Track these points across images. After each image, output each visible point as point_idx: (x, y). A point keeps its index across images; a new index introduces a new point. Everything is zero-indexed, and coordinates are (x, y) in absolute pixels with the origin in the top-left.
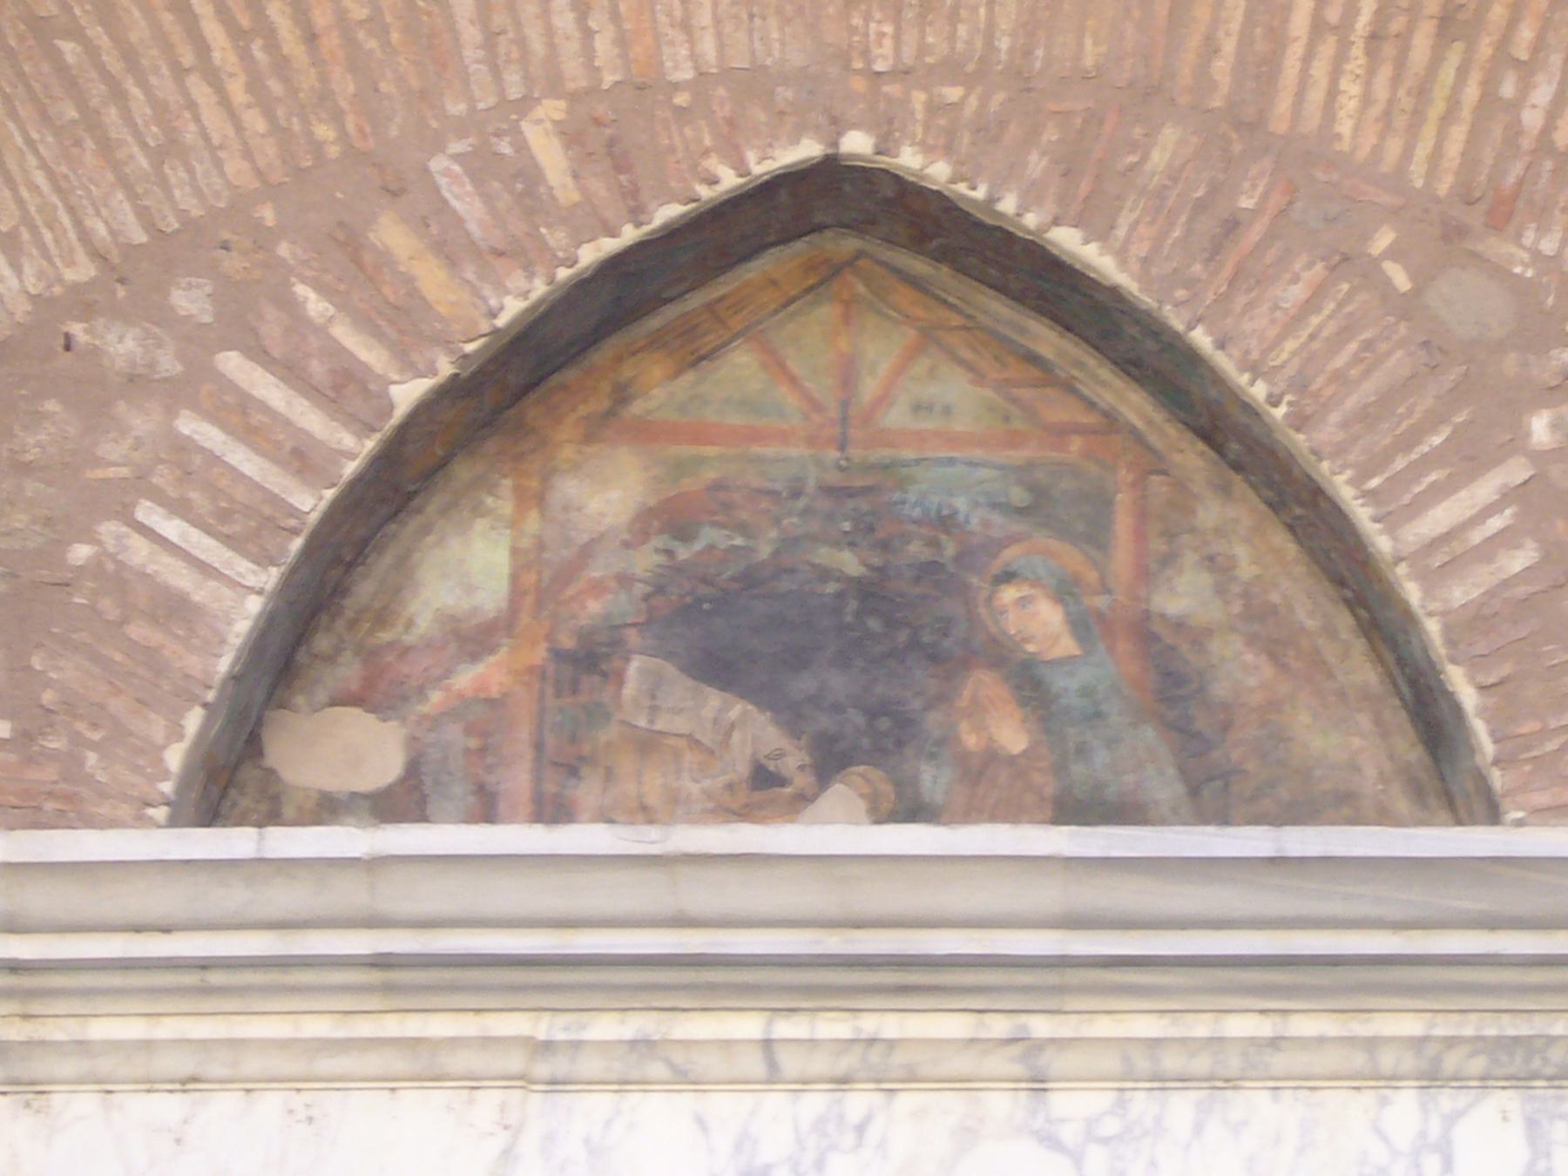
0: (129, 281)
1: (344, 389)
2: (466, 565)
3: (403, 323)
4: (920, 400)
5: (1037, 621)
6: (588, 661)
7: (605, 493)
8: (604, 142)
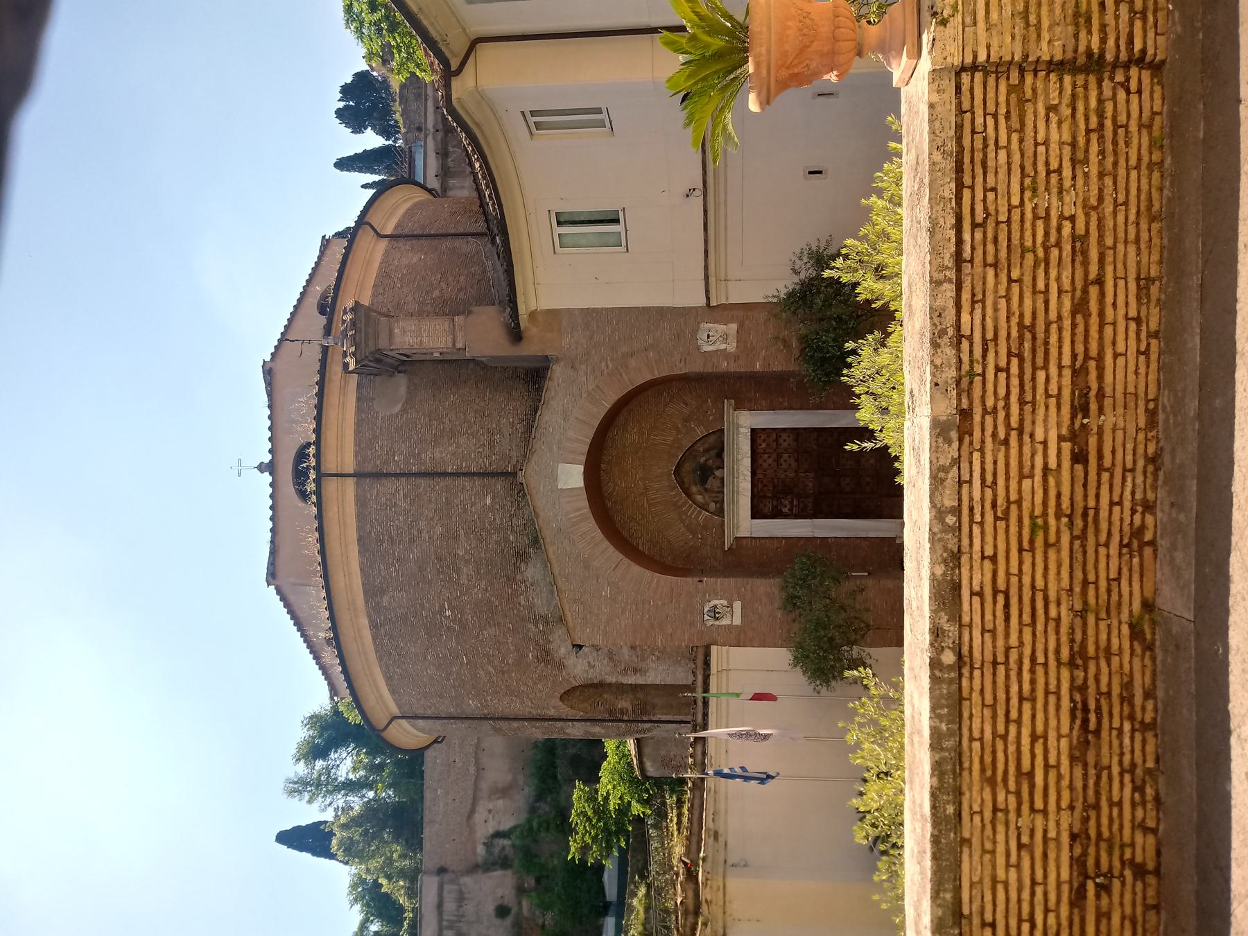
0: (683, 521)
1: (691, 506)
2: (699, 498)
3: (685, 503)
4: (688, 467)
5: (703, 460)
6: (706, 490)
7: (694, 489)
8: (673, 489)
